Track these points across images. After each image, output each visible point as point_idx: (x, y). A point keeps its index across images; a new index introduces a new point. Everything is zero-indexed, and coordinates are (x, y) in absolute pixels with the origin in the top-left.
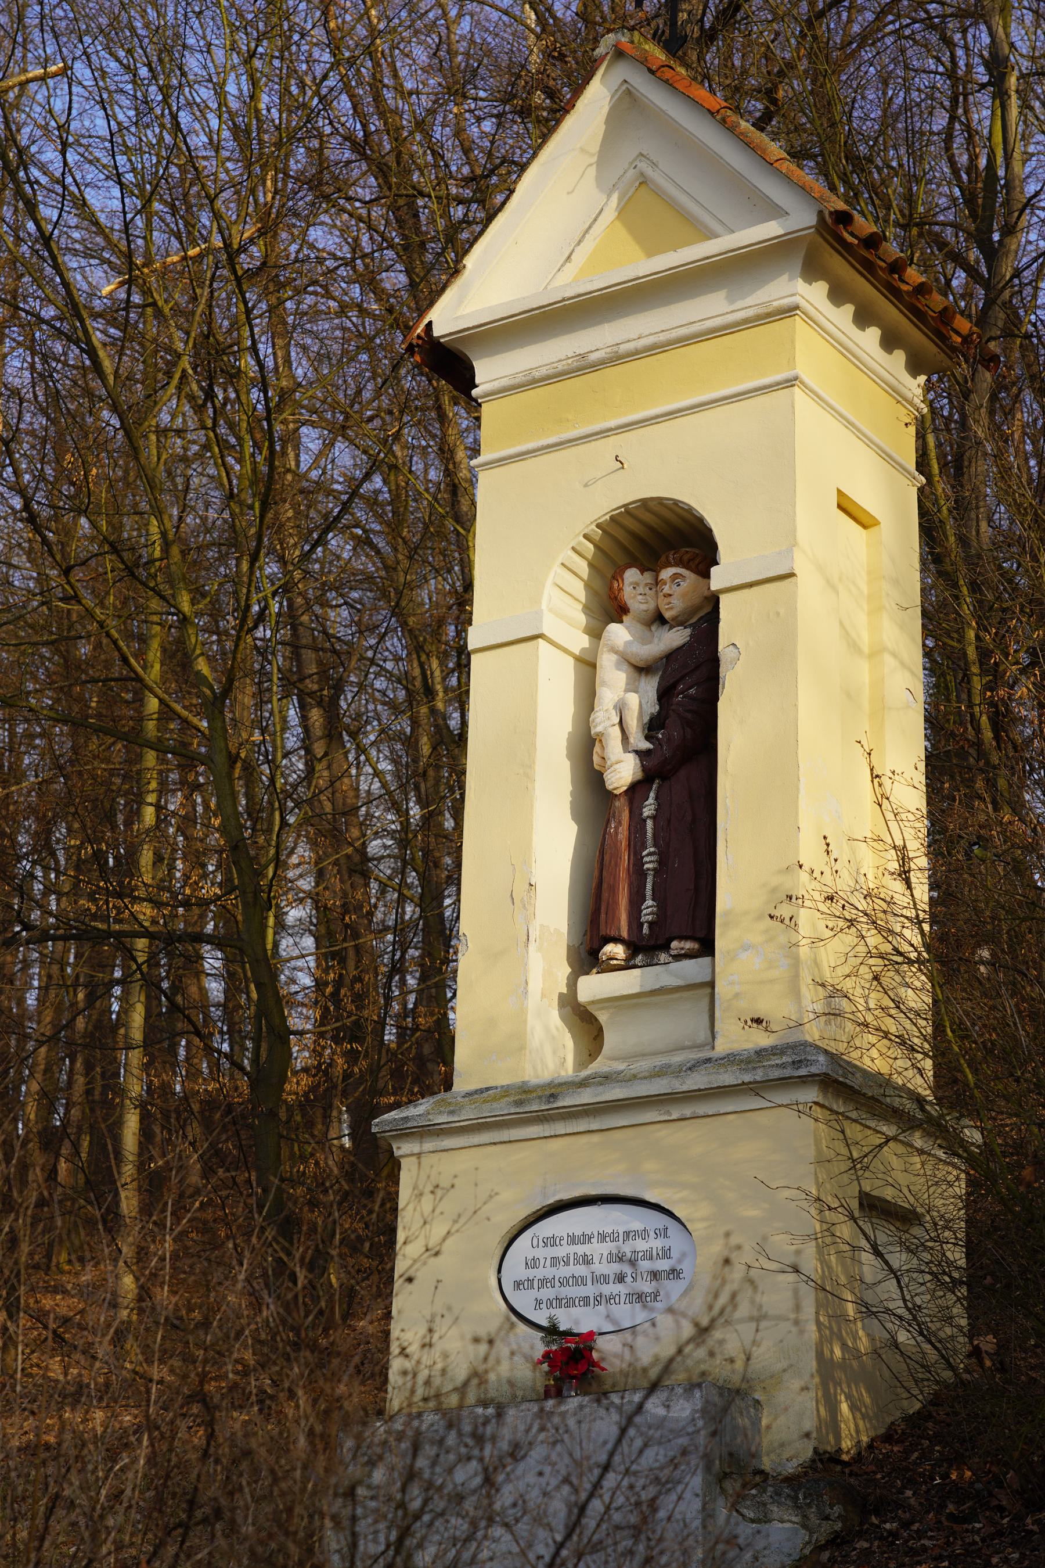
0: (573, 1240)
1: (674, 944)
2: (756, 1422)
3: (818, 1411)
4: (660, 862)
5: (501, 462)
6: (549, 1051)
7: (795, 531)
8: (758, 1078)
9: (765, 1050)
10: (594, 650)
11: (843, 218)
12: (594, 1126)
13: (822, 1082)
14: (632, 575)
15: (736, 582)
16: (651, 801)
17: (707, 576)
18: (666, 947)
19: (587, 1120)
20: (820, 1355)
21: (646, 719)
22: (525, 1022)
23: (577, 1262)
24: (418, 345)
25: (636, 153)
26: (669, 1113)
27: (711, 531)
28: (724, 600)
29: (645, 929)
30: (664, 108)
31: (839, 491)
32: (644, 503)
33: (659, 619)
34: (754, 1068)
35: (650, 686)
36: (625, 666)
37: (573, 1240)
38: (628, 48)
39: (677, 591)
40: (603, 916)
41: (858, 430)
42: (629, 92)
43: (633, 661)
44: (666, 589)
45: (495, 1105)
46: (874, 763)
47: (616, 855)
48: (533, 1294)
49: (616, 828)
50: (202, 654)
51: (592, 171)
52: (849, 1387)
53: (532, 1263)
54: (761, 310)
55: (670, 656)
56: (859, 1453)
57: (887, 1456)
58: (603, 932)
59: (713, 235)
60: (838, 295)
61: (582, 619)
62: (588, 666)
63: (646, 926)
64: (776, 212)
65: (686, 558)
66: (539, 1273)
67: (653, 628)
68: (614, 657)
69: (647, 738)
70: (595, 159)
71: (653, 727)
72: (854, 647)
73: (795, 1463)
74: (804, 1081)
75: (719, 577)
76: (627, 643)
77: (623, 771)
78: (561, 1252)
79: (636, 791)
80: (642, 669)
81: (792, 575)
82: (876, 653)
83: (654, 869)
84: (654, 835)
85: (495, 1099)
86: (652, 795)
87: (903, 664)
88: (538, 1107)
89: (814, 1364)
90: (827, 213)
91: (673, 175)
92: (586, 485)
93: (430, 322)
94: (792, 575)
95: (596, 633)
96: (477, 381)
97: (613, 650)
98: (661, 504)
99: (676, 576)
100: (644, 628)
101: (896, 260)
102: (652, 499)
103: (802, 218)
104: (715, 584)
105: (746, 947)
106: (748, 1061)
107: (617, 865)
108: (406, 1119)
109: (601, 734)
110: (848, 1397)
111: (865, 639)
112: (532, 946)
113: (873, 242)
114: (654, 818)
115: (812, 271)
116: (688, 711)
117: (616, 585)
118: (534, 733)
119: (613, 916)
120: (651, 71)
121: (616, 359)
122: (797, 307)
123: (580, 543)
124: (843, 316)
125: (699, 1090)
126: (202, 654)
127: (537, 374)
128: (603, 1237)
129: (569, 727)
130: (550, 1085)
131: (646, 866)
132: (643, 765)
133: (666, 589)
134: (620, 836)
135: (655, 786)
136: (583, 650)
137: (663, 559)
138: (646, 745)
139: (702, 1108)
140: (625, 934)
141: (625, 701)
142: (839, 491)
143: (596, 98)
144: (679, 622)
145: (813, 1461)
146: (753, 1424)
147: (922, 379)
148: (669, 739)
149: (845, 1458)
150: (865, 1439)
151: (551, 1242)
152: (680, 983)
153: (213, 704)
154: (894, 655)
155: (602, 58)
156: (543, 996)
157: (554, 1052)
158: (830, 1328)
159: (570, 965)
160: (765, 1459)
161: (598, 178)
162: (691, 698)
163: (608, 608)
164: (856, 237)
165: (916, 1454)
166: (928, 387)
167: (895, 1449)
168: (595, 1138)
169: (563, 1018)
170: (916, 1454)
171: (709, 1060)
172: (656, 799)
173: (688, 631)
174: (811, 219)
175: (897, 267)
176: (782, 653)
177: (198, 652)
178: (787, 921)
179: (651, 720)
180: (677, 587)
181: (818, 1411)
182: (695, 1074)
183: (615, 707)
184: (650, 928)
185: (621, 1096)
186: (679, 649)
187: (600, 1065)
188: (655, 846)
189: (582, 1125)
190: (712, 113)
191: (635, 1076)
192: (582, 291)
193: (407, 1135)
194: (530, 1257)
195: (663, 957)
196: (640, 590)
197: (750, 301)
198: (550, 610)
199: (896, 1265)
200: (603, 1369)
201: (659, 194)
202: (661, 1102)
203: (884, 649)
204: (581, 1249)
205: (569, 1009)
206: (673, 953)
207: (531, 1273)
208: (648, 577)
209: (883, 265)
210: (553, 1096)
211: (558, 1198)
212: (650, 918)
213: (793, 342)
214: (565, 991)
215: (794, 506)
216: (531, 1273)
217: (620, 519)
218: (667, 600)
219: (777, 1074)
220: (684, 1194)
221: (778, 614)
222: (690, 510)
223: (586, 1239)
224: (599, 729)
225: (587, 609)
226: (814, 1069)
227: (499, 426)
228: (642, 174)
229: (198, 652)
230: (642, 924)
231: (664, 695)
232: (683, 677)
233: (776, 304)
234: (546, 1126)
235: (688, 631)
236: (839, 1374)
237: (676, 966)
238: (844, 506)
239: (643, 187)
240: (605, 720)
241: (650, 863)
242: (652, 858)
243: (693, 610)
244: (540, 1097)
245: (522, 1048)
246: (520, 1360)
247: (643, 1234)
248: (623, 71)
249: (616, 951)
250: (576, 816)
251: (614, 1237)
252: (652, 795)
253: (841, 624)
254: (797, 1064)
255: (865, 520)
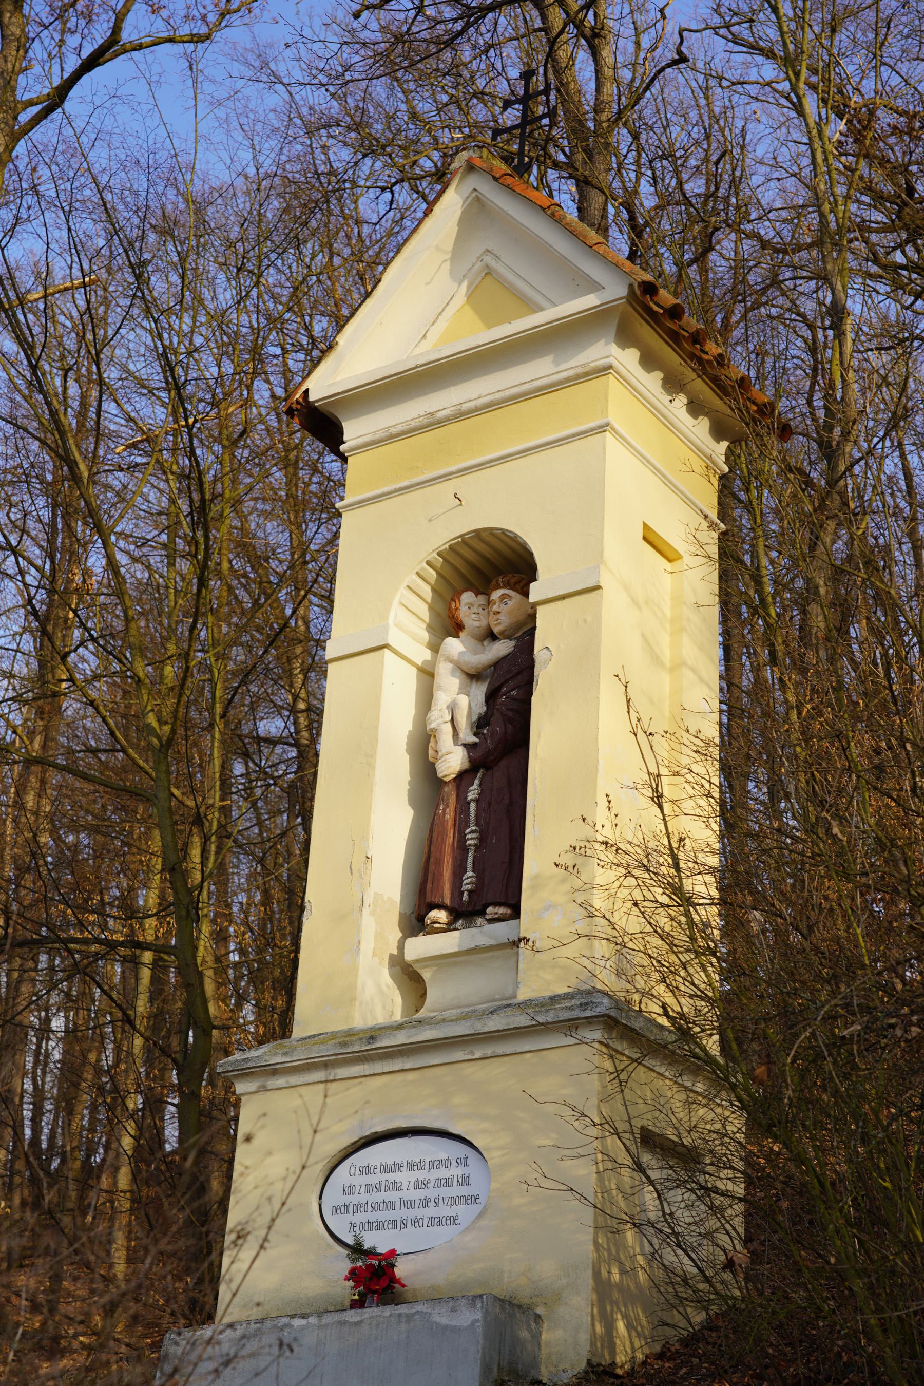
0: (385, 1168)
1: (490, 910)
2: (536, 1336)
3: (593, 1325)
4: (481, 839)
5: (361, 503)
6: (377, 1000)
7: (602, 551)
8: (550, 1020)
9: (559, 996)
10: (433, 663)
11: (649, 289)
12: (408, 1065)
13: (605, 1023)
14: (468, 597)
15: (551, 595)
16: (475, 786)
17: (526, 594)
18: (482, 913)
19: (401, 1059)
20: (597, 1274)
21: (475, 718)
22: (357, 976)
23: (388, 1188)
24: (297, 410)
25: (483, 249)
26: (472, 1053)
27: (531, 554)
28: (541, 612)
29: (465, 897)
30: (505, 208)
31: (645, 525)
32: (478, 533)
33: (491, 636)
34: (547, 1011)
35: (480, 691)
36: (459, 673)
37: (385, 1168)
38: (478, 162)
39: (504, 609)
40: (429, 885)
41: (665, 476)
42: (478, 199)
43: (465, 668)
44: (495, 608)
45: (322, 1047)
46: (630, 695)
47: (444, 833)
48: (349, 1218)
49: (444, 810)
50: (153, 710)
51: (447, 265)
52: (626, 1306)
53: (348, 1190)
54: (580, 370)
55: (497, 664)
56: (633, 1368)
57: (658, 1371)
58: (428, 900)
59: (542, 309)
60: (649, 361)
61: (425, 636)
62: (427, 674)
63: (466, 894)
64: (594, 287)
65: (513, 581)
66: (354, 1199)
67: (485, 643)
68: (450, 666)
69: (475, 734)
70: (449, 256)
71: (480, 725)
72: (656, 659)
73: (570, 1373)
74: (589, 1021)
75: (536, 591)
76: (461, 654)
77: (452, 760)
78: (373, 1179)
79: (463, 778)
80: (473, 676)
81: (598, 588)
82: (677, 666)
83: (475, 845)
84: (477, 816)
85: (323, 1042)
86: (477, 782)
87: (701, 680)
88: (364, 1050)
89: (591, 1282)
90: (636, 285)
91: (515, 267)
92: (430, 520)
93: (307, 390)
94: (598, 588)
95: (435, 648)
96: (345, 438)
97: (449, 660)
98: (492, 534)
99: (503, 596)
100: (476, 642)
101: (697, 331)
102: (484, 530)
103: (615, 290)
104: (532, 598)
105: (549, 907)
106: (542, 1005)
107: (443, 841)
108: (246, 1060)
109: (434, 730)
110: (625, 1317)
111: (667, 656)
112: (366, 911)
113: (675, 313)
114: (477, 801)
115: (625, 338)
116: (510, 710)
117: (453, 605)
118: (377, 728)
119: (438, 887)
120: (496, 179)
121: (460, 415)
122: (610, 367)
123: (423, 569)
124: (652, 382)
125: (499, 1031)
126: (153, 710)
127: (394, 431)
128: (411, 1166)
129: (410, 727)
130: (373, 1029)
131: (468, 842)
132: (469, 757)
133: (495, 608)
134: (447, 817)
135: (479, 775)
136: (425, 662)
137: (494, 582)
138: (473, 739)
139: (501, 1048)
140: (448, 901)
141: (457, 701)
142: (645, 525)
143: (452, 202)
144: (507, 635)
145: (586, 1372)
146: (533, 1336)
147: (725, 444)
148: (492, 734)
149: (619, 1372)
150: (640, 1356)
151: (367, 1170)
152: (493, 942)
153: (160, 750)
154: (694, 670)
155: (457, 171)
156: (374, 955)
157: (384, 1007)
158: (609, 1250)
159: (402, 930)
160: (543, 1369)
161: (452, 272)
162: (513, 698)
163: (448, 625)
164: (661, 307)
165: (684, 1370)
166: (729, 453)
167: (667, 1365)
168: (411, 1076)
169: (392, 976)
170: (684, 1370)
171: (509, 1006)
172: (480, 785)
173: (512, 643)
174: (623, 291)
175: (697, 338)
176: (588, 654)
177: (149, 708)
178: (570, 869)
179: (479, 719)
180: (504, 605)
181: (593, 1325)
182: (495, 1017)
183: (448, 708)
184: (469, 895)
185: (431, 1038)
186: (505, 658)
187: (422, 1014)
188: (477, 825)
189: (397, 1065)
190: (543, 209)
191: (444, 1020)
192: (432, 358)
193: (247, 1075)
194: (347, 1185)
195: (480, 921)
196: (475, 609)
197: (573, 363)
198: (396, 625)
199: (653, 1178)
200: (403, 1286)
201: (501, 281)
202: (466, 1042)
203: (684, 664)
204: (391, 1177)
205: (398, 968)
206: (487, 917)
207: (347, 1199)
208: (481, 599)
209: (686, 334)
210: (372, 1038)
211: (373, 1130)
212: (469, 887)
213: (606, 396)
214: (395, 952)
215: (602, 530)
216: (347, 1199)
217: (458, 549)
218: (496, 617)
219: (566, 1015)
220: (485, 1125)
221: (585, 621)
222: (515, 538)
223: (397, 1167)
224: (433, 725)
225: (430, 628)
226: (599, 1010)
227: (361, 475)
228: (487, 266)
229: (149, 708)
230: (462, 893)
231: (491, 697)
232: (506, 681)
233: (593, 365)
234: (366, 1066)
235: (512, 643)
236: (616, 1295)
237: (490, 927)
238: (651, 538)
239: (488, 277)
240: (439, 718)
241: (471, 840)
242: (474, 835)
243: (518, 626)
244: (361, 1039)
245: (353, 999)
246: (333, 1274)
247: (446, 1163)
248: (475, 182)
249: (441, 916)
250: (413, 802)
251: (420, 1166)
252: (477, 782)
253: (643, 635)
254: (583, 1006)
255: (670, 555)
